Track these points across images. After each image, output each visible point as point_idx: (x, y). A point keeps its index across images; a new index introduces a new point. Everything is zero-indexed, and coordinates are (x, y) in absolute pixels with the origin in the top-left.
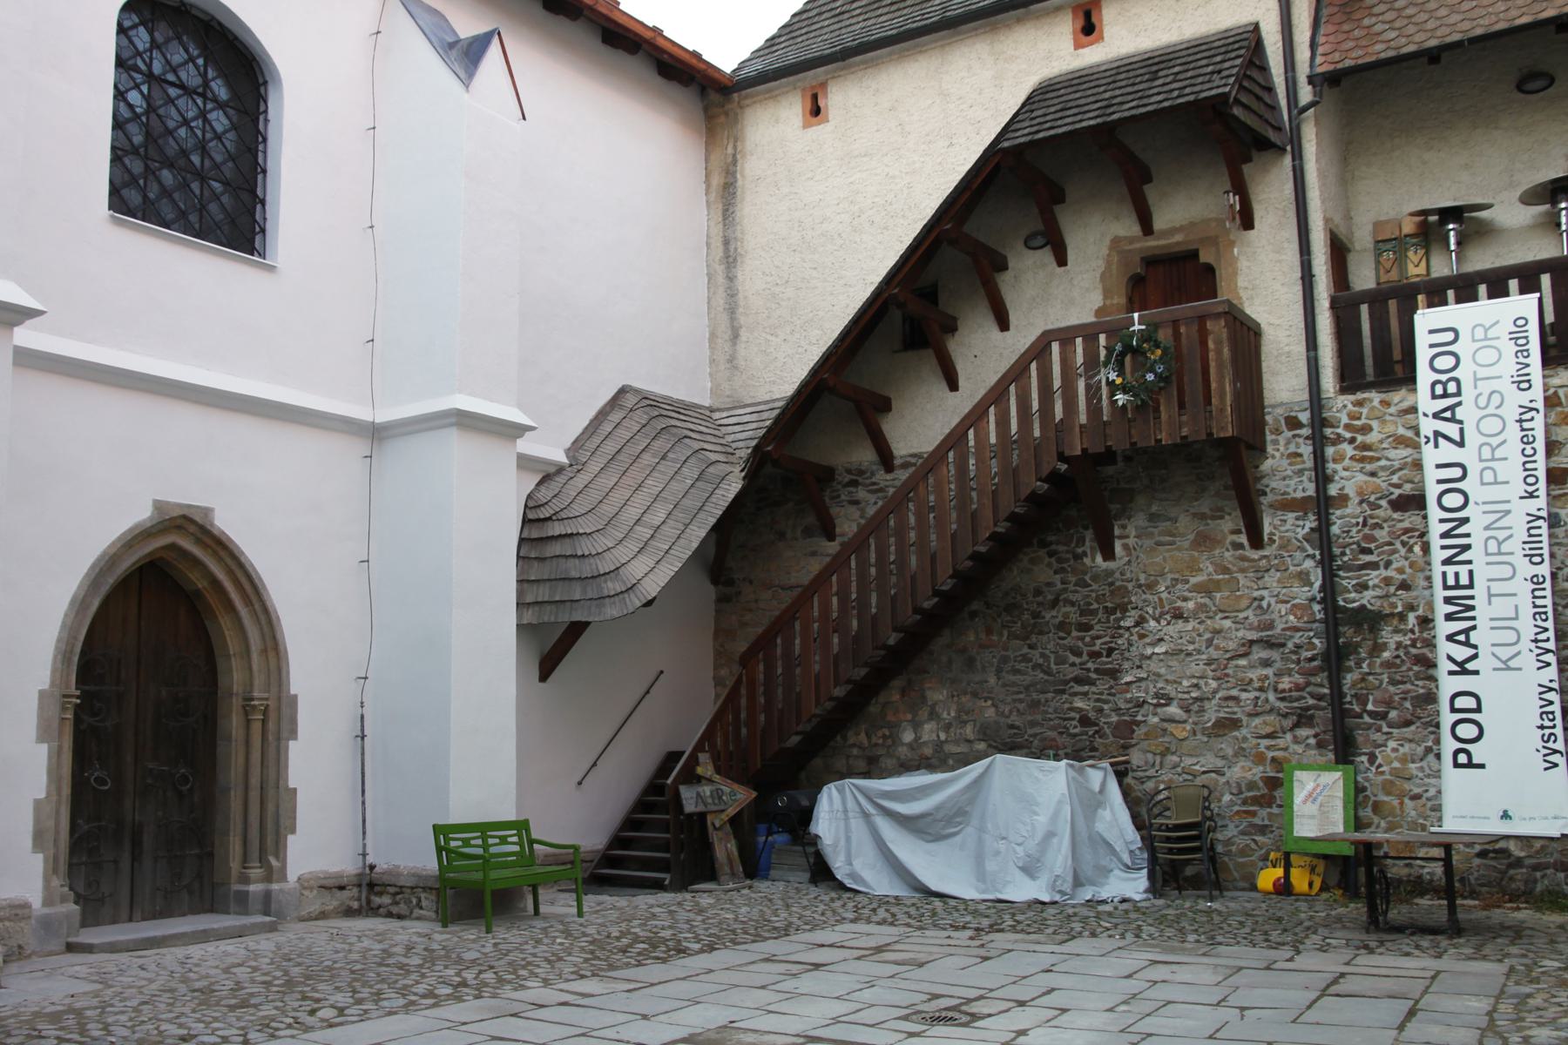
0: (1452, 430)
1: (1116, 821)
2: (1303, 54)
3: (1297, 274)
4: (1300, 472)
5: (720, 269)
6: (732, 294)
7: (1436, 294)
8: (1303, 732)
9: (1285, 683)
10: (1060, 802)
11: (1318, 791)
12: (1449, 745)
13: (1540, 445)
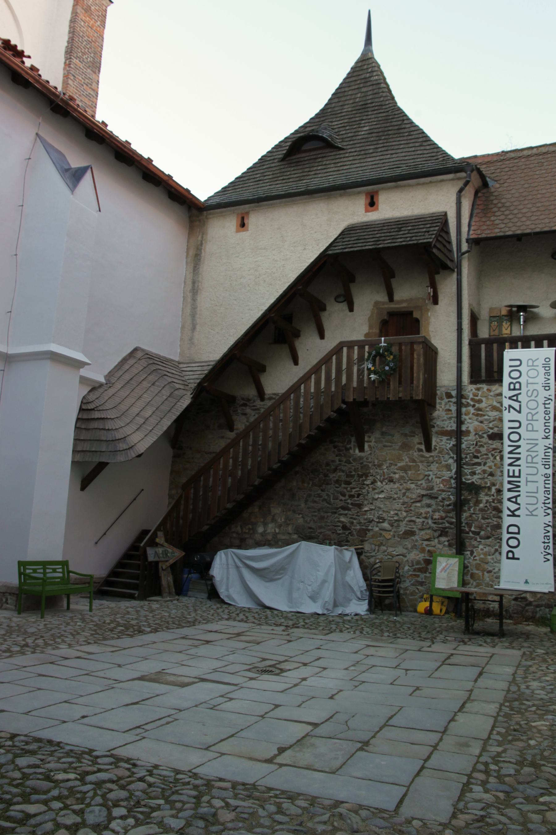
0: (516, 405)
2: (465, 228)
3: (455, 327)
5: (189, 295)
6: (194, 308)
7: (514, 343)
8: (443, 539)
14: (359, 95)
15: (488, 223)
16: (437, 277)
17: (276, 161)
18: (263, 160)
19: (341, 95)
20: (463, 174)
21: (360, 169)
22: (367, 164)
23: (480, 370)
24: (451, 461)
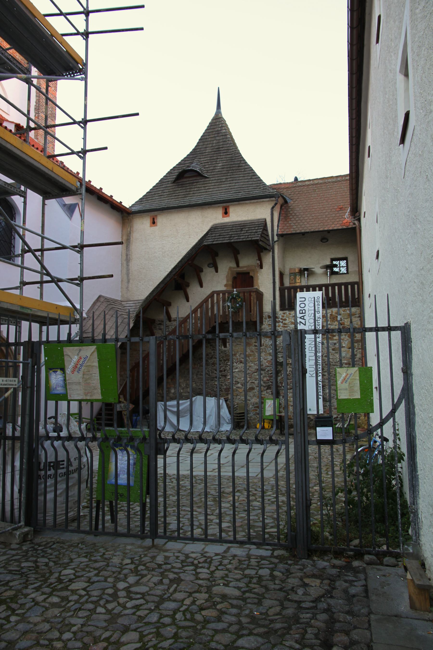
0: (303, 321)
1: (225, 412)
2: (275, 228)
5: (125, 263)
6: (128, 270)
8: (269, 391)
9: (265, 379)
10: (213, 408)
11: (81, 363)
14: (215, 142)
15: (288, 225)
16: (262, 254)
17: (170, 183)
18: (161, 181)
19: (205, 140)
20: (274, 199)
21: (219, 192)
23: (285, 303)
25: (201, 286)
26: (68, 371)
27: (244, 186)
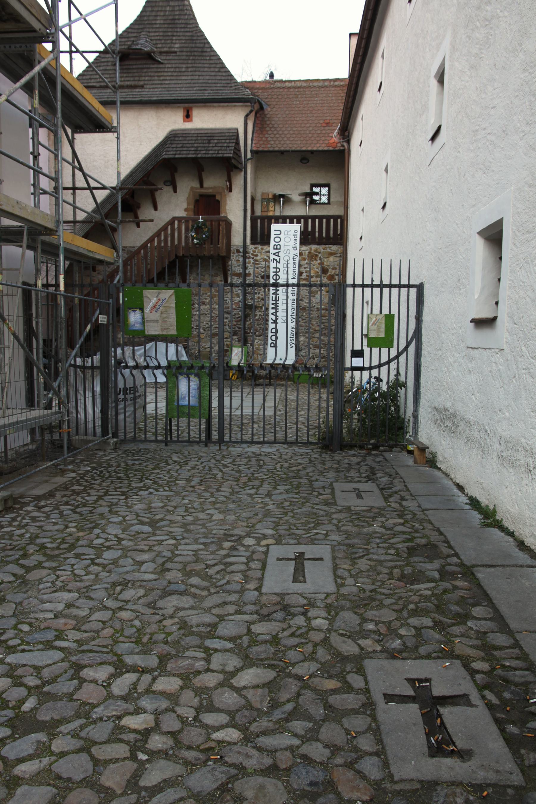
2: (249, 142)
3: (243, 208)
4: (239, 266)
7: (278, 219)
12: (270, 341)
13: (297, 265)
15: (264, 139)
16: (232, 173)
17: (110, 64)
20: (249, 104)
21: (178, 86)
22: (182, 82)
24: (239, 292)
25: (156, 209)
26: (147, 311)
27: (210, 81)
